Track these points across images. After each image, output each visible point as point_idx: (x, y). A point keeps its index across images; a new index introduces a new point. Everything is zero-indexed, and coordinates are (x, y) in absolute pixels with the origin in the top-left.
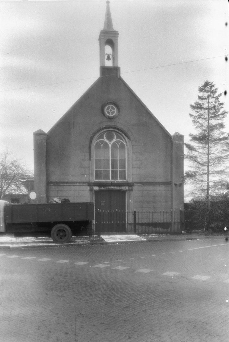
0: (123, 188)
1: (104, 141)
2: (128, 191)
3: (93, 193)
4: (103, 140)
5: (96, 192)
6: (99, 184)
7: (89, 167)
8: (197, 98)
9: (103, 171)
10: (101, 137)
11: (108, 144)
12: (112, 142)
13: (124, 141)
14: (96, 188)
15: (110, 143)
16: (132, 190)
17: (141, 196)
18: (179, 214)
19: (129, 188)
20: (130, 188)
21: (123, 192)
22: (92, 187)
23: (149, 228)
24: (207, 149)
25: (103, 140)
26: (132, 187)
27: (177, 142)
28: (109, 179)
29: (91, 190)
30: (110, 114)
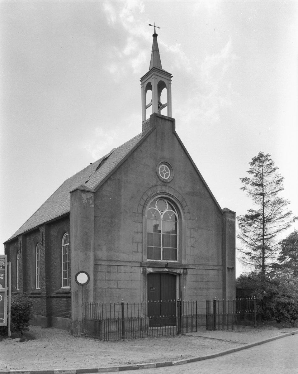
0: (178, 271)
1: (156, 210)
2: (183, 275)
3: (145, 277)
4: (155, 209)
5: (150, 274)
6: (152, 265)
7: (142, 243)
8: (249, 165)
9: (154, 247)
10: (153, 204)
11: (164, 215)
12: (164, 212)
13: (175, 211)
14: (150, 270)
15: (162, 214)
16: (185, 274)
17: (195, 282)
18: (222, 303)
19: (183, 271)
20: (185, 271)
21: (174, 276)
22: (146, 269)
23: (140, 314)
24: (262, 230)
25: (155, 209)
26: (187, 270)
27: (230, 219)
28: (160, 259)
29: (144, 273)
30: (163, 177)
